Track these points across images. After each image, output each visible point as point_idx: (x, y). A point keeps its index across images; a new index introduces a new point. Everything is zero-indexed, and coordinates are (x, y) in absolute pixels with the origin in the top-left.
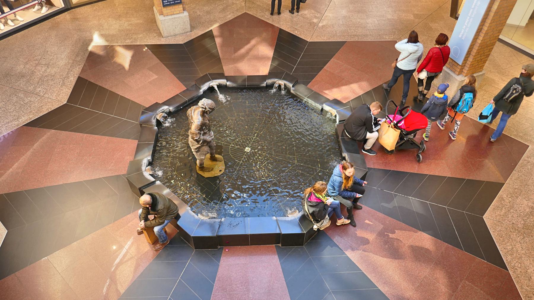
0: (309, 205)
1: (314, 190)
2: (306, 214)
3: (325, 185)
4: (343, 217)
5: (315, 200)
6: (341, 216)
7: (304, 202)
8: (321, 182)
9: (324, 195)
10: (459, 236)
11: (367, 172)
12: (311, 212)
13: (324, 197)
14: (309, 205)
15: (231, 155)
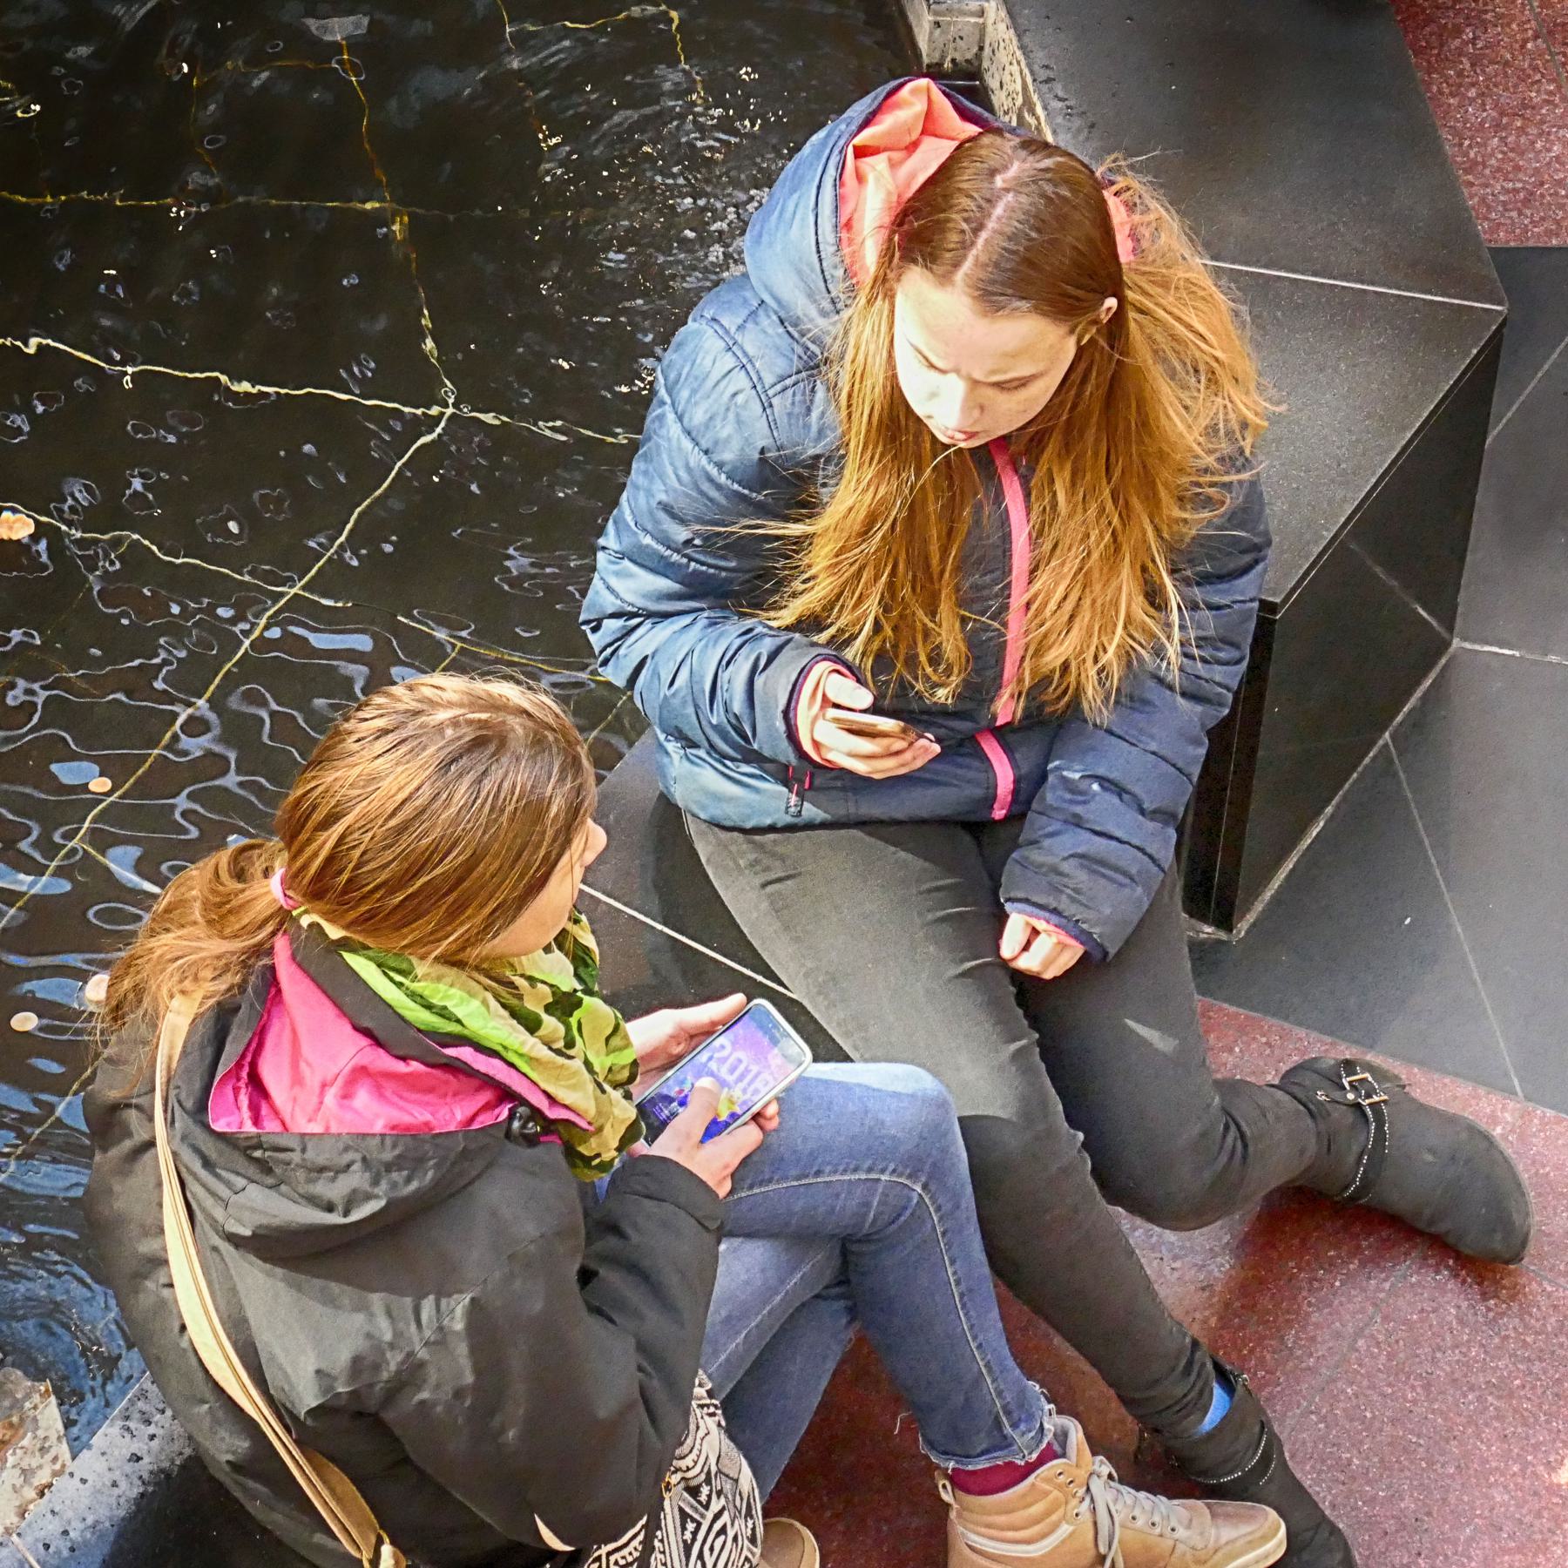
0: (235, 1240)
1: (318, 890)
2: (225, 1447)
3: (538, 743)
4: (1076, 1434)
5: (363, 1098)
6: (1021, 1412)
7: (126, 1198)
8: (450, 686)
9: (559, 972)
10: (1341, 786)
11: (1493, 350)
12: (307, 1398)
13: (563, 1005)
14: (235, 1240)
15: (992, 618)
